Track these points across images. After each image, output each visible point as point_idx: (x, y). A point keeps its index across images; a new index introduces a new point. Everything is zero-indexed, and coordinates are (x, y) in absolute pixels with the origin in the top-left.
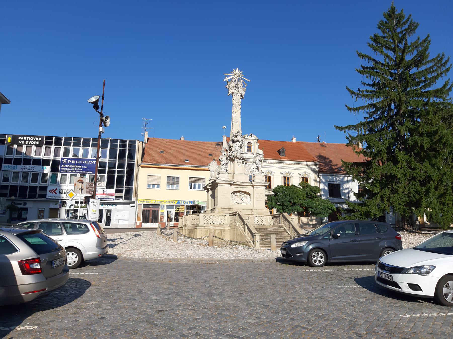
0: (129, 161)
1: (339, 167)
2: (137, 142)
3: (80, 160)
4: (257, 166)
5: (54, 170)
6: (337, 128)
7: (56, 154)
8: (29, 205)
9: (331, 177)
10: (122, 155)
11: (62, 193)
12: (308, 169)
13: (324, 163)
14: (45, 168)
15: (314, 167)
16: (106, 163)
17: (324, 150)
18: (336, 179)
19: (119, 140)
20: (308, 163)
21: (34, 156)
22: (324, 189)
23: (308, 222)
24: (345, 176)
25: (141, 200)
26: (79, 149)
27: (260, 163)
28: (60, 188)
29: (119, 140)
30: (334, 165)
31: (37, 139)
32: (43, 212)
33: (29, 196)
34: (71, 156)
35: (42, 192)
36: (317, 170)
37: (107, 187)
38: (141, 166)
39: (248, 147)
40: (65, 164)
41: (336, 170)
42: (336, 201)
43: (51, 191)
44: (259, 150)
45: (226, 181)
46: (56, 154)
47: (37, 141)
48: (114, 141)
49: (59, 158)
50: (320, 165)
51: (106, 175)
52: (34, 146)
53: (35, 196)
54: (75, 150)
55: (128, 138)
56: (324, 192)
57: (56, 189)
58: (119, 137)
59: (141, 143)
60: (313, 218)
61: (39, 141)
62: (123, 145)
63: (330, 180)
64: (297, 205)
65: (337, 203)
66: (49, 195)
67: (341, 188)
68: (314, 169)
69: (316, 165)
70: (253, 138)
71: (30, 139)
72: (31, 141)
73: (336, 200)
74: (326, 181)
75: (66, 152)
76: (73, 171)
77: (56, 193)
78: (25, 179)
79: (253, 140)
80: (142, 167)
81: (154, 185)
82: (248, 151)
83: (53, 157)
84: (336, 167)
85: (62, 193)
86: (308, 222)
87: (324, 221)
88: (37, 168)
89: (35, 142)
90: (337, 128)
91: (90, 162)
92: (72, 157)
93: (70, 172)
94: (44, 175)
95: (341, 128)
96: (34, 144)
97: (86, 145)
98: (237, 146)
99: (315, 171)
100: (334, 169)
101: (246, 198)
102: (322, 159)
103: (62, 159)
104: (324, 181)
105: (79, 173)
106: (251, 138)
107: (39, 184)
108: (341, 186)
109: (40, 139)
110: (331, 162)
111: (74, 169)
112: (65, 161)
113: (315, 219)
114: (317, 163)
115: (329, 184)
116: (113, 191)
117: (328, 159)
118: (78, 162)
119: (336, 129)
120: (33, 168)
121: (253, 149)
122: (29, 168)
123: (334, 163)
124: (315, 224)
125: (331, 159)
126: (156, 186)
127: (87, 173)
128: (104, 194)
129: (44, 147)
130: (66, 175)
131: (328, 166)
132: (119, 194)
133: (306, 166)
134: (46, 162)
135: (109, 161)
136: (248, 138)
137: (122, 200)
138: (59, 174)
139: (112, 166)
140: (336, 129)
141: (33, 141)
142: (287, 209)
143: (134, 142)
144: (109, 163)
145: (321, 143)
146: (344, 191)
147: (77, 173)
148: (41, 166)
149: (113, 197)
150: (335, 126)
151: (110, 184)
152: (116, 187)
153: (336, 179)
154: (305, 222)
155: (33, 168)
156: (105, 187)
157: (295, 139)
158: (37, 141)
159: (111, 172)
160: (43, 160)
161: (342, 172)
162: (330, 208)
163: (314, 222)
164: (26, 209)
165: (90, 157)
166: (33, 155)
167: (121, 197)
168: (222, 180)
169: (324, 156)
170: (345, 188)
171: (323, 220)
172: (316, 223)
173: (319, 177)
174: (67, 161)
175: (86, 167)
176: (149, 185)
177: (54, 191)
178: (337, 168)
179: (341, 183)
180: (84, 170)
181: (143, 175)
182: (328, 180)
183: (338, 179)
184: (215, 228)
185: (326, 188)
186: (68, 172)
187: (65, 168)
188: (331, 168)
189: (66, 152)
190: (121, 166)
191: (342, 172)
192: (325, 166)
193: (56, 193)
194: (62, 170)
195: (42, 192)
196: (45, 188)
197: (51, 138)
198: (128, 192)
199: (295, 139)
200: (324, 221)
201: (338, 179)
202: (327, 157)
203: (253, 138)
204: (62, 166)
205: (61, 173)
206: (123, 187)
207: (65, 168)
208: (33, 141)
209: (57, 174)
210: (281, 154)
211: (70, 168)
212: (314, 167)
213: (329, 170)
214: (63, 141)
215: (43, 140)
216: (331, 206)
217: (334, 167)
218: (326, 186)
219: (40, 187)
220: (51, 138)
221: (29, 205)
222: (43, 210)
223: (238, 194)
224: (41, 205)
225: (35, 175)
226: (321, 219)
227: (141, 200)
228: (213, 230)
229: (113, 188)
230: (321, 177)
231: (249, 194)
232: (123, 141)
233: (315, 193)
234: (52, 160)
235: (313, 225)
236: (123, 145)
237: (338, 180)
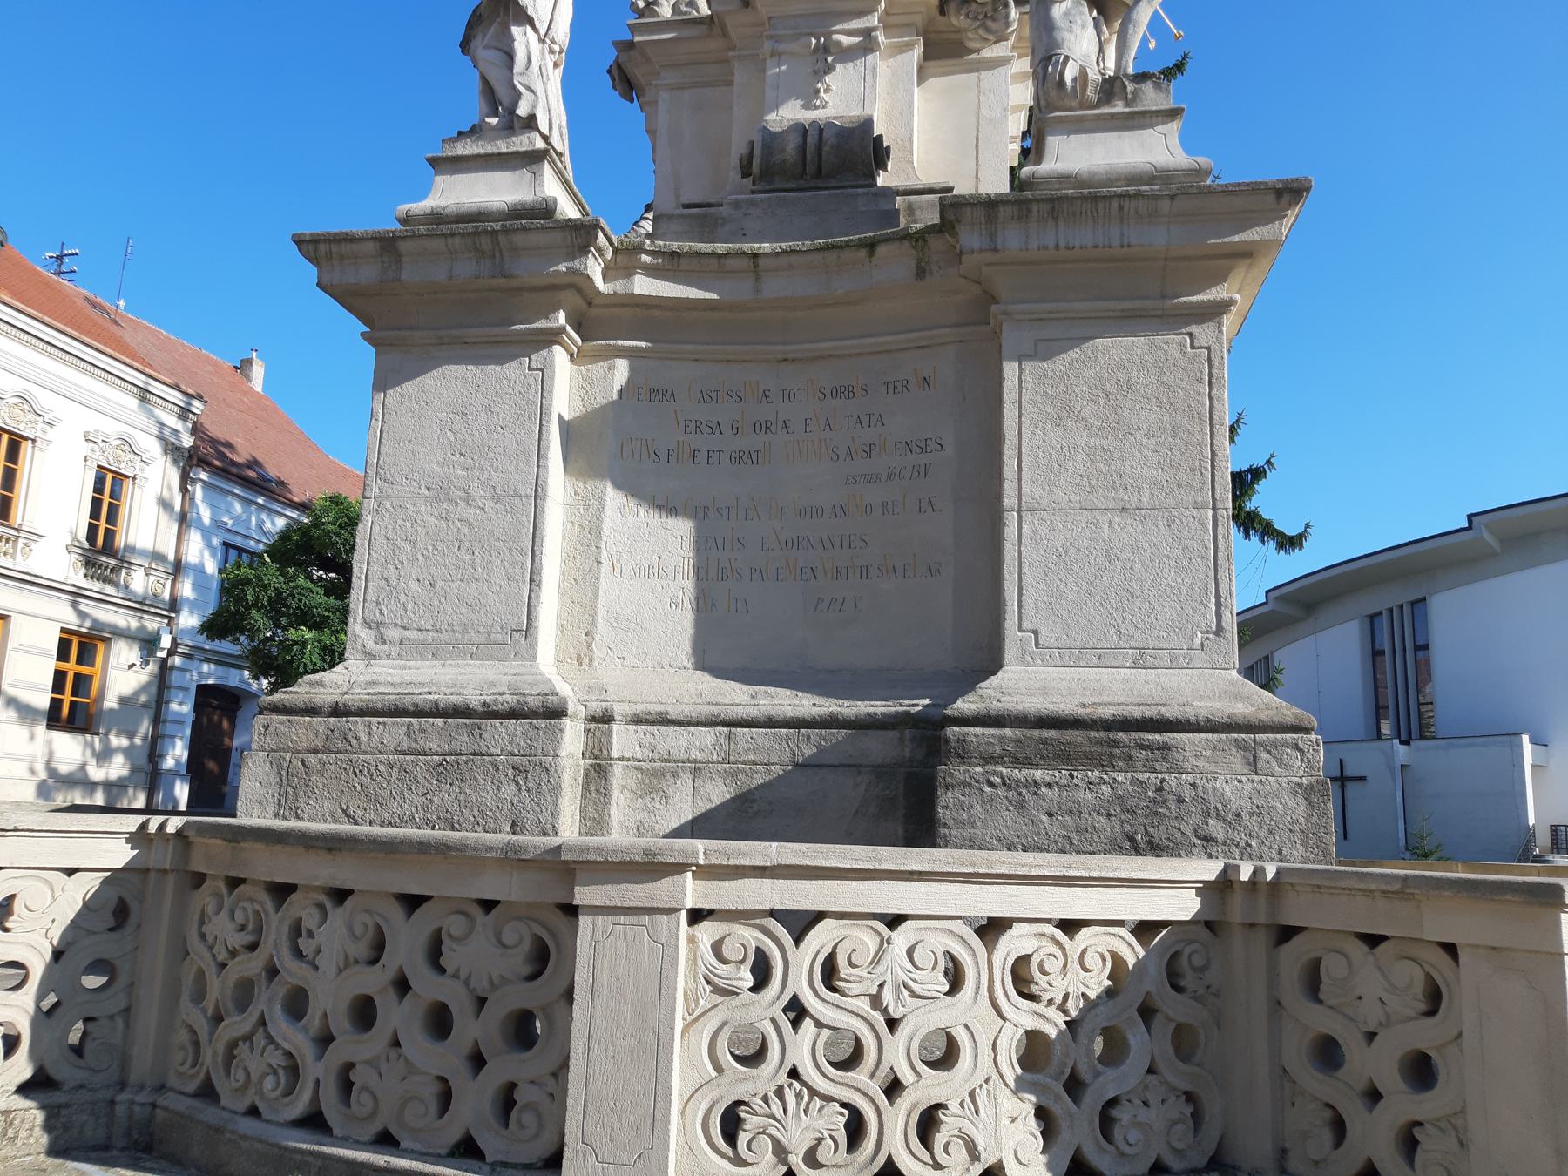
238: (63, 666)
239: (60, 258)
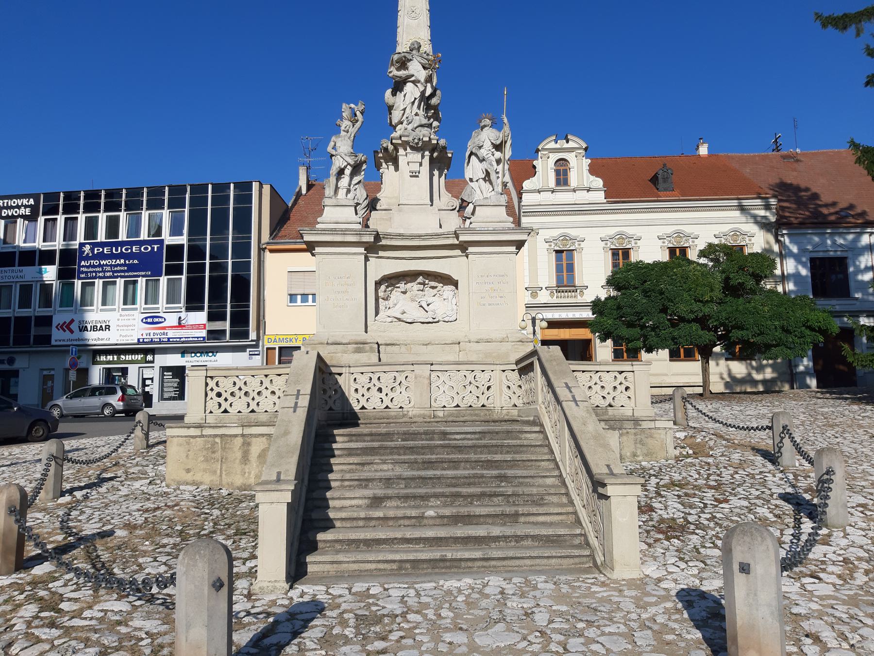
0: (238, 238)
1: (842, 210)
2: (255, 186)
3: (122, 244)
4: (485, 165)
5: (66, 274)
6: (829, 22)
7: (69, 234)
8: (20, 363)
9: (816, 239)
10: (220, 227)
11: (86, 329)
12: (744, 219)
13: (795, 202)
14: (46, 272)
15: (762, 213)
16: (183, 245)
17: (795, 170)
18: (834, 243)
19: (210, 186)
20: (745, 203)
21: (22, 245)
22: (796, 277)
23: (749, 374)
24: (861, 234)
25: (273, 338)
26: (118, 217)
27: (498, 155)
28: (82, 317)
29: (210, 186)
30: (826, 206)
31: (25, 202)
32: (51, 378)
33: (17, 343)
34: (101, 237)
35: (42, 331)
36: (773, 219)
37: (188, 309)
38: (268, 247)
39: (558, 172)
40: (87, 258)
41: (833, 218)
42: (838, 308)
43: (62, 327)
44: (592, 178)
45: (344, 232)
46: (69, 234)
47: (26, 207)
48: (199, 190)
49: (75, 245)
50: (783, 208)
51: (184, 278)
52: (20, 221)
53: (26, 342)
54: (109, 218)
55: (231, 177)
56: (796, 284)
57: (72, 321)
58: (209, 178)
59: (267, 189)
60: (765, 362)
61: (30, 206)
62: (221, 199)
63: (816, 245)
64: (689, 322)
65: (839, 315)
66: (58, 336)
67: (851, 269)
68: (765, 217)
69: (767, 207)
70: (571, 144)
71: (11, 203)
72: (13, 208)
73: (837, 304)
74: (803, 251)
75: (91, 227)
76: (108, 274)
77: (72, 332)
78: (25, 302)
79: (571, 150)
80: (271, 251)
81: (305, 296)
82: (558, 183)
83: (62, 242)
84: (832, 210)
85: (86, 329)
86: (749, 374)
87: (801, 368)
88: (28, 273)
89: (22, 211)
90: (829, 22)
91: (146, 249)
92: (104, 240)
93: (100, 278)
94: (46, 288)
95: (841, 22)
96: (19, 216)
97: (133, 206)
98: (409, 99)
99: (765, 225)
100: (825, 216)
101: (441, 301)
102: (786, 191)
103: (82, 245)
104: (795, 249)
105: (122, 277)
106: (566, 146)
107: (36, 310)
108: (850, 261)
109: (32, 202)
110: (815, 196)
111: (108, 268)
112: (87, 248)
113: (771, 366)
114: (773, 201)
115: (812, 260)
116: (200, 317)
117: (807, 189)
118: (116, 250)
119: (824, 26)
120: (19, 274)
121: (574, 179)
122: (11, 274)
123: (825, 198)
124: (773, 381)
125: (814, 190)
126: (299, 297)
127: (138, 276)
128: (180, 326)
129: (41, 220)
130: (93, 284)
131: (807, 209)
132: (217, 326)
133: (737, 213)
134: (47, 257)
135: (189, 240)
136: (558, 146)
137: (227, 341)
138: (78, 284)
139: (196, 252)
140: (824, 26)
141: (18, 207)
142: (658, 336)
143: (248, 186)
144: (189, 246)
145: (784, 152)
146: (860, 277)
147: (117, 277)
148: (36, 268)
149: (203, 333)
150: (818, 16)
151: (193, 303)
152: (209, 307)
153: (834, 243)
154: (739, 376)
155: (19, 274)
156: (183, 309)
157: (706, 145)
158: (26, 207)
159: (196, 270)
160: (40, 251)
161: (852, 220)
162: (816, 325)
163: (769, 374)
164: (16, 373)
165: (144, 235)
166: (20, 241)
167: (223, 332)
168: (333, 231)
169: (795, 182)
170: (863, 266)
171: (797, 366)
172: (774, 375)
173: (777, 241)
174: (92, 250)
175: (136, 262)
176: (292, 297)
177: (66, 326)
178: (836, 213)
179: (849, 254)
180: (131, 268)
181: (278, 273)
182: (809, 247)
183: (840, 241)
184: (247, 431)
185: (804, 272)
186: (95, 278)
187: (88, 267)
188: (817, 214)
189: (91, 227)
190: (219, 252)
191: (852, 220)
192: (799, 208)
193: (72, 332)
194: (83, 272)
195: (42, 331)
196: (46, 321)
197: (55, 196)
198: (240, 320)
199: (706, 145)
200: (801, 368)
201: (840, 241)
202: (803, 185)
203: (571, 144)
204: (83, 263)
205: (80, 282)
206: (226, 307)
207: (88, 267)
208: (18, 207)
209: (73, 283)
210: (661, 185)
211: (100, 266)
212: (762, 213)
213: (809, 217)
214: (82, 202)
215: (37, 202)
216: (817, 317)
217: (825, 211)
218: (804, 265)
219: (37, 318)
220: (55, 196)
221: (20, 363)
222: (52, 372)
223: (413, 287)
224: (47, 362)
225: (26, 290)
226: (791, 365)
227: (273, 338)
228: (239, 441)
229: (201, 309)
230: (787, 240)
231: (455, 284)
232: (221, 189)
233: (758, 278)
234: (61, 251)
235: (764, 382)
236: (221, 199)
237: (841, 245)
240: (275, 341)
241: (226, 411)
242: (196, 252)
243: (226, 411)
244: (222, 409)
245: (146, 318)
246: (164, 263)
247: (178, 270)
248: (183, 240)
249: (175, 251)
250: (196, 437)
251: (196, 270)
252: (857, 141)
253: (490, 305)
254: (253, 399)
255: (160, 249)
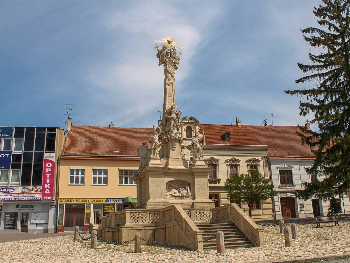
6: (288, 92)
90: (288, 92)
139: (28, 158)
159: (27, 166)
238: (95, 176)
239: (265, 121)
240: (63, 201)
241: (136, 223)
242: (28, 158)
243: (136, 223)
244: (135, 222)
245: (2, 189)
246: (11, 163)
247: (18, 166)
248: (21, 152)
249: (17, 158)
250: (130, 230)
251: (27, 166)
252: (301, 142)
253: (199, 191)
254: (144, 219)
255: (10, 156)
